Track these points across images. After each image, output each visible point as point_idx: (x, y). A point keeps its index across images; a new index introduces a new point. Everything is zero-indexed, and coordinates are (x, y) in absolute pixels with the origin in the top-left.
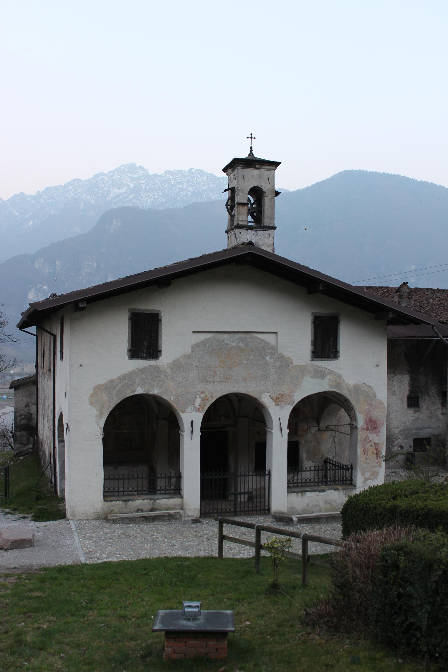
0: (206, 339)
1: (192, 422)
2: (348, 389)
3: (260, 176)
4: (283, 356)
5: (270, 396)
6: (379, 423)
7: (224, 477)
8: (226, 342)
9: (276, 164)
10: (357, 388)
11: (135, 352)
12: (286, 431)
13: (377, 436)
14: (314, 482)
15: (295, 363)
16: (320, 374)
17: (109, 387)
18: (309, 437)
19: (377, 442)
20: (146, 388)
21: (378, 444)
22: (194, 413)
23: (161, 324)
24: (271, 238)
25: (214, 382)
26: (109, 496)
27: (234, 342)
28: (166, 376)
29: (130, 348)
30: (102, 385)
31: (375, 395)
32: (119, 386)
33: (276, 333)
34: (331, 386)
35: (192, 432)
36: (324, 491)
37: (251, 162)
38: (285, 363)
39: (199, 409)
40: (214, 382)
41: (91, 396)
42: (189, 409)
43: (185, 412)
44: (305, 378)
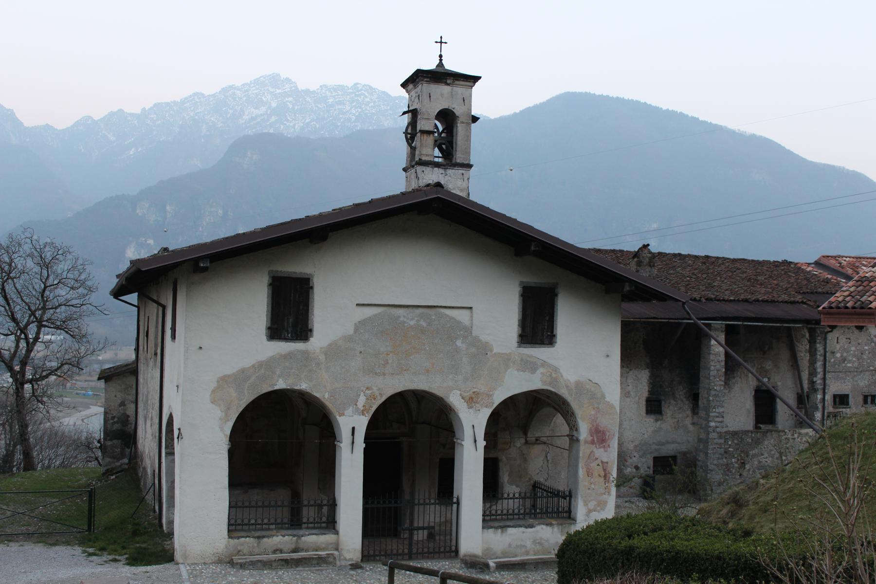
0: (375, 315)
1: (353, 428)
2: (567, 387)
3: (452, 95)
4: (480, 341)
5: (461, 395)
6: (608, 434)
8: (402, 319)
9: (474, 79)
10: (579, 387)
11: (275, 332)
12: (482, 443)
15: (495, 351)
16: (530, 366)
17: (239, 378)
20: (290, 381)
22: (356, 417)
24: (466, 179)
25: (384, 374)
27: (412, 319)
28: (318, 364)
29: (269, 325)
30: (229, 376)
31: (603, 396)
32: (253, 378)
33: (471, 308)
34: (544, 382)
35: (353, 443)
36: (532, 526)
37: (440, 76)
38: (482, 350)
39: (363, 411)
40: (384, 374)
41: (213, 391)
42: (349, 411)
43: (343, 414)
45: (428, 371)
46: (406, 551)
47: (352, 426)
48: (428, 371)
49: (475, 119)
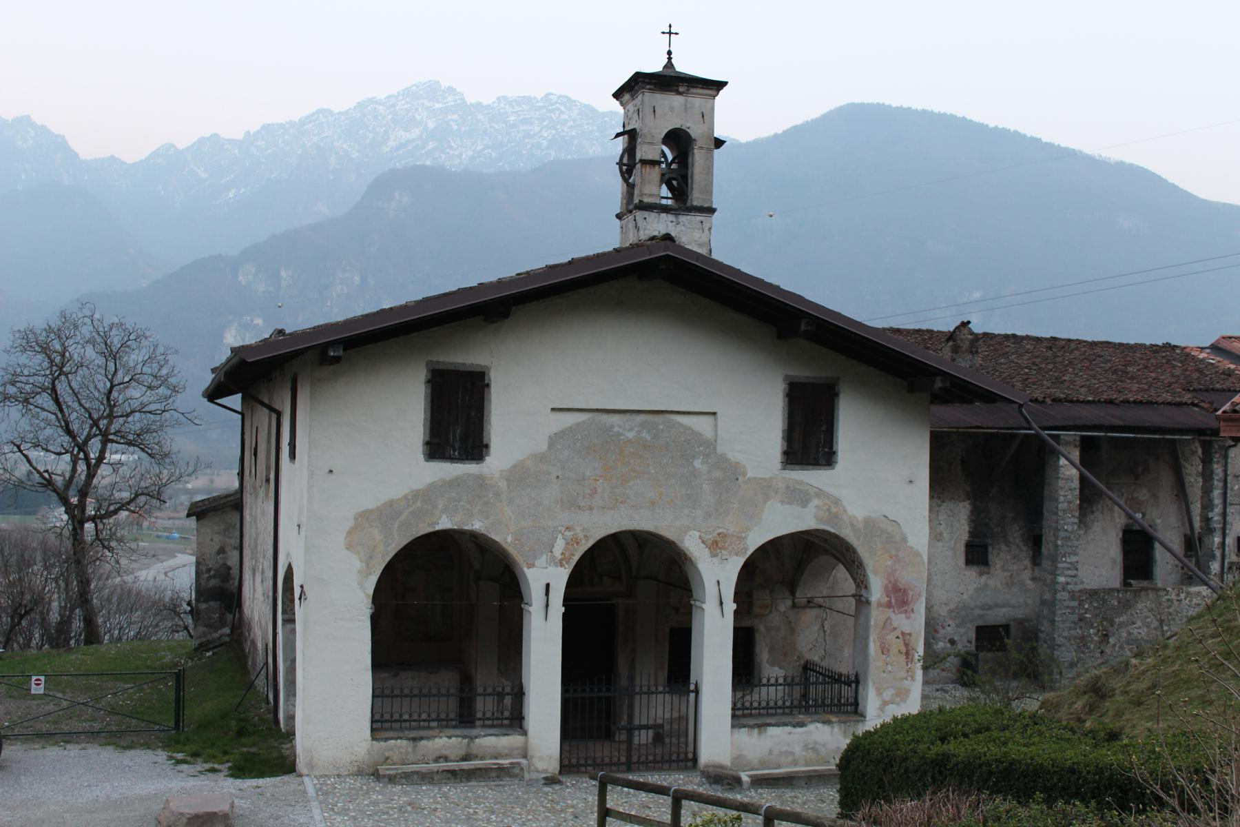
0: (578, 424)
1: (548, 586)
2: (852, 526)
3: (686, 108)
4: (728, 460)
5: (700, 537)
7: (608, 694)
8: (616, 429)
11: (436, 449)
12: (730, 607)
13: (908, 618)
14: (783, 708)
15: (749, 475)
16: (798, 496)
17: (385, 514)
18: (775, 619)
19: (907, 630)
21: (910, 634)
22: (552, 569)
23: (489, 393)
25: (591, 509)
26: (382, 729)
27: (631, 430)
28: (497, 494)
29: (428, 439)
33: (714, 414)
35: (547, 606)
36: (802, 725)
37: (668, 81)
38: (730, 473)
39: (561, 560)
40: (591, 509)
41: (350, 533)
42: (542, 560)
44: (769, 503)
45: (653, 503)
46: (623, 759)
47: (546, 582)
48: (653, 503)
49: (719, 143)
